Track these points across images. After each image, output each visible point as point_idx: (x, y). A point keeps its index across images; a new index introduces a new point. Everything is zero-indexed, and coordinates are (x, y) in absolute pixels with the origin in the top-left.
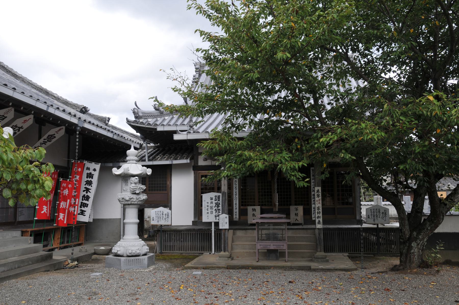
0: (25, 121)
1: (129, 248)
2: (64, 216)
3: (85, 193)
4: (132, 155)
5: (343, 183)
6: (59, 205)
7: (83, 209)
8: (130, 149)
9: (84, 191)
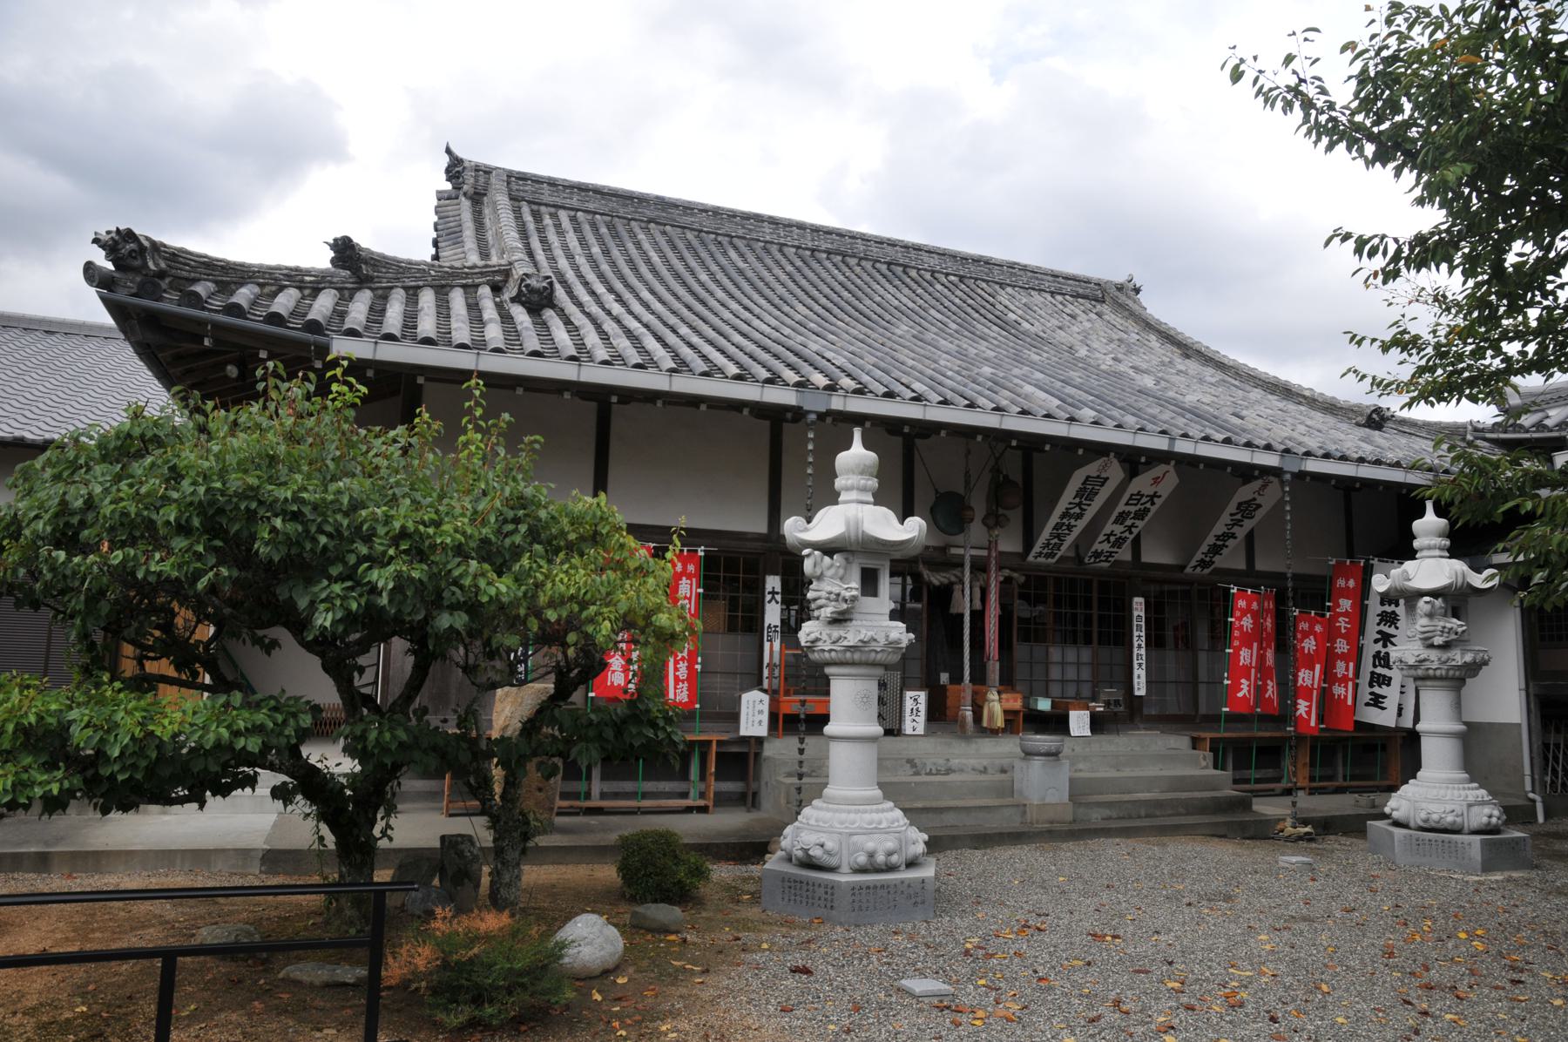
0: (1156, 481)
1: (1424, 805)
2: (1310, 707)
3: (1379, 647)
4: (1428, 534)
5: (357, 635)
6: (1296, 677)
7: (1377, 690)
8: (1421, 514)
9: (1376, 641)
